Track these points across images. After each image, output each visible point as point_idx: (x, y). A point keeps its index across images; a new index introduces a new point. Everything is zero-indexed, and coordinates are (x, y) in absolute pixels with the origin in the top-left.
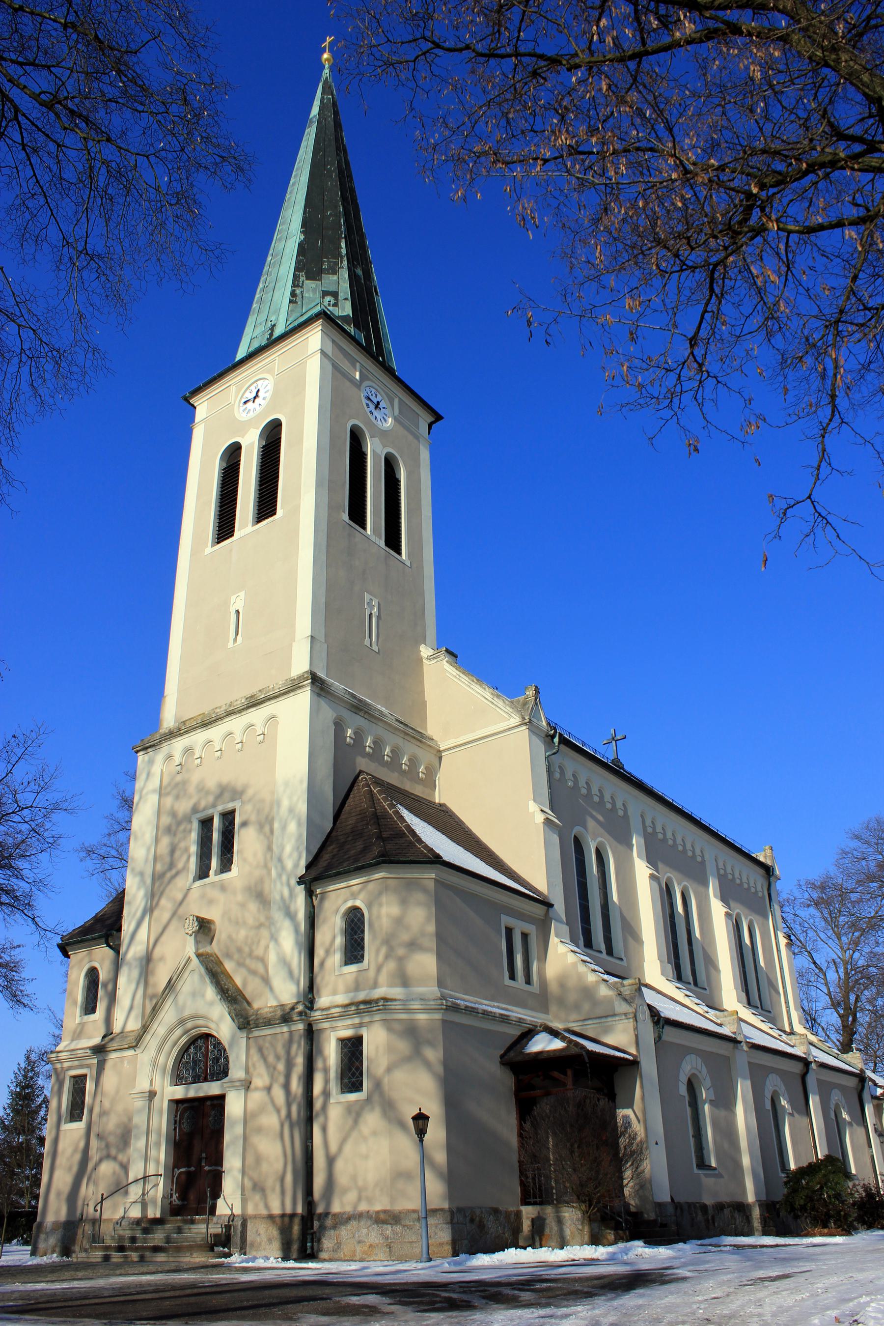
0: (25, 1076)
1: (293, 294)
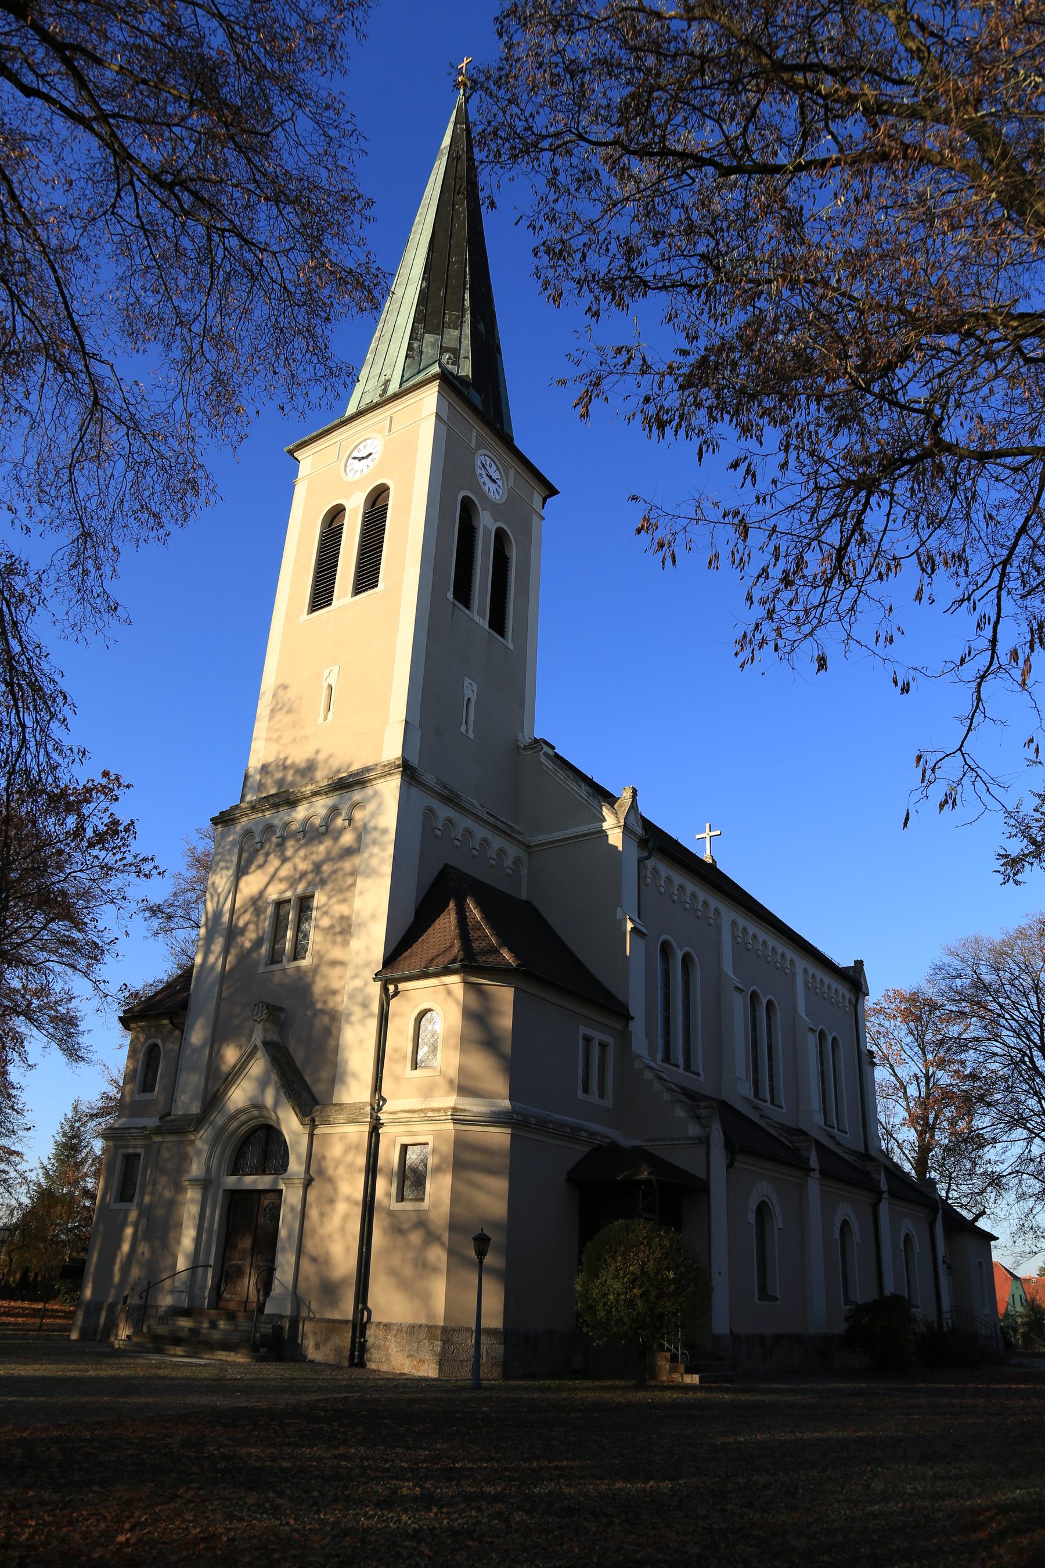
0: (72, 1127)
1: (410, 347)
